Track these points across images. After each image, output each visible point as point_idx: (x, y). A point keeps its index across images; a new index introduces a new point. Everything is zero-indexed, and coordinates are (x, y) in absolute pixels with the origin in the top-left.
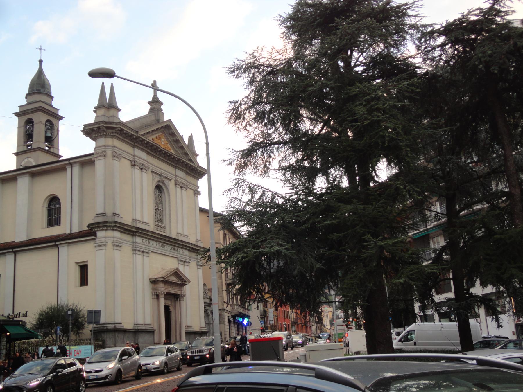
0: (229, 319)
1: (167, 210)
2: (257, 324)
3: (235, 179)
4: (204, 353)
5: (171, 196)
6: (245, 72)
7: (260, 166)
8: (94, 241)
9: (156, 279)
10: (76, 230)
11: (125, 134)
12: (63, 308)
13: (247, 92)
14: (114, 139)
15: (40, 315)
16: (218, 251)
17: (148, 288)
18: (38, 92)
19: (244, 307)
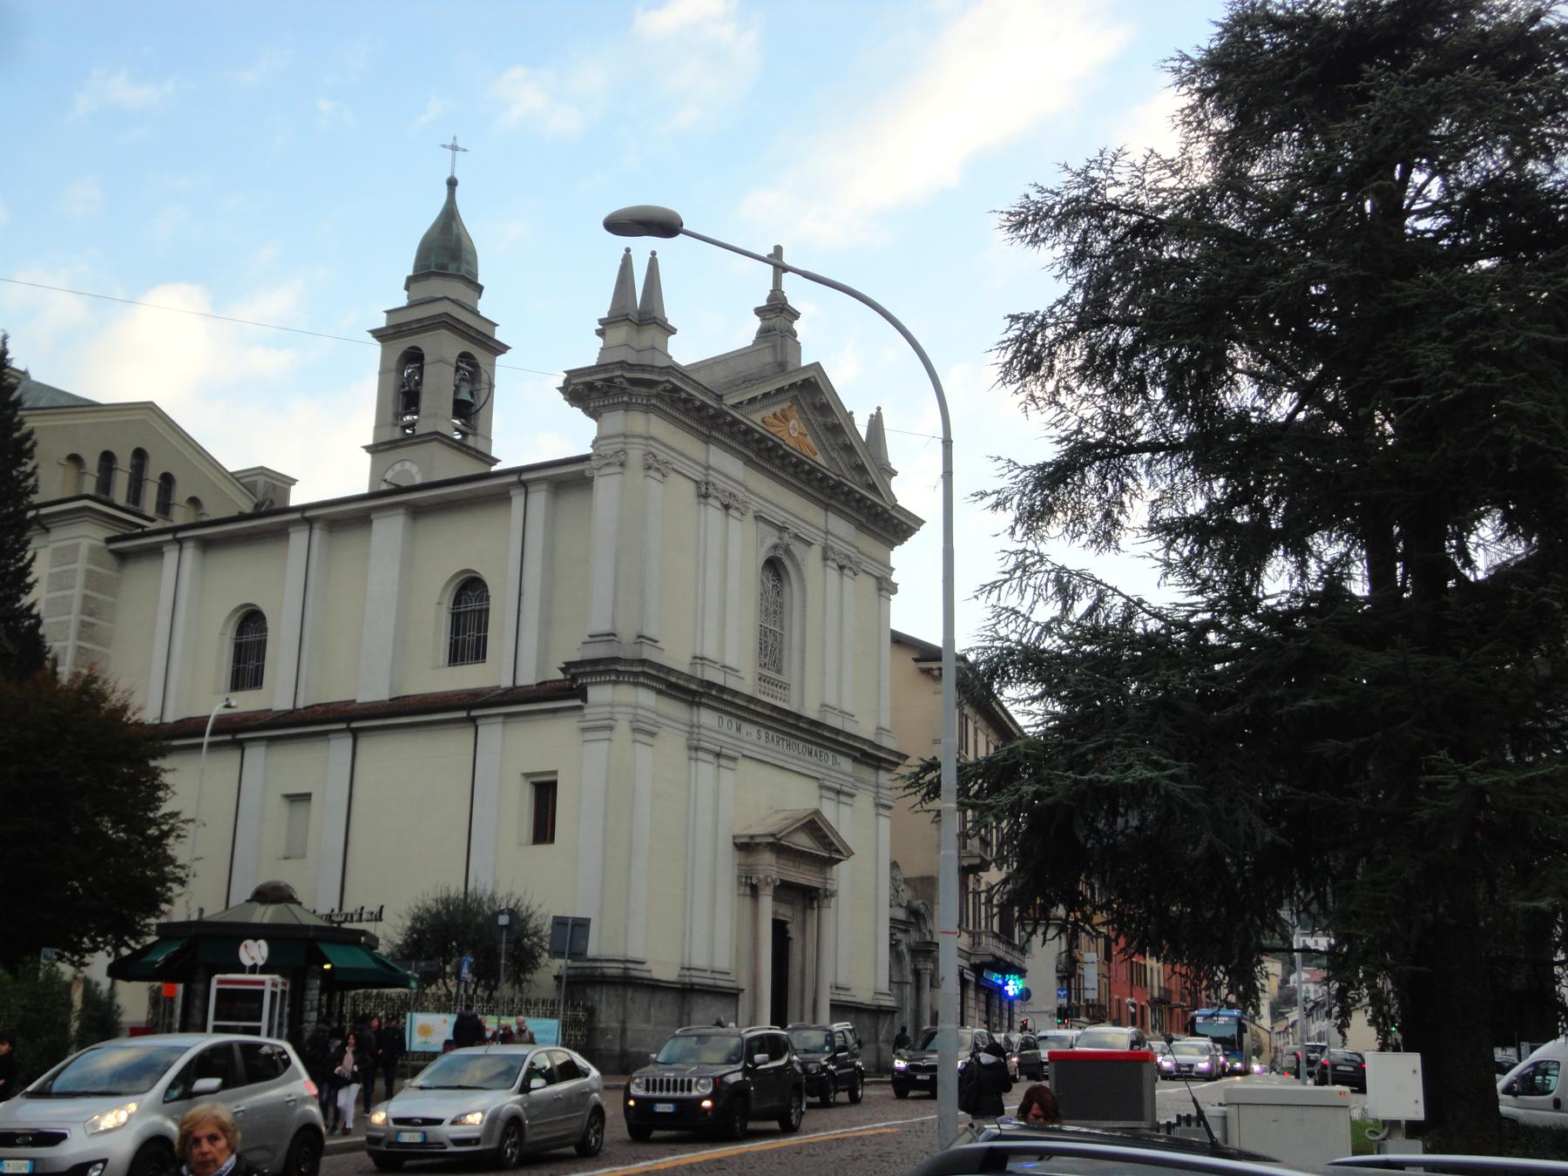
0: (961, 974)
1: (796, 632)
2: (1048, 994)
3: (1016, 553)
4: (695, 1093)
5: (809, 594)
6: (1058, 227)
7: (1093, 515)
8: (579, 713)
9: (752, 837)
10: (528, 678)
11: (685, 401)
12: (480, 902)
13: (1063, 288)
14: (653, 417)
15: (416, 918)
16: (965, 774)
17: (728, 862)
18: (441, 273)
19: (1009, 943)
